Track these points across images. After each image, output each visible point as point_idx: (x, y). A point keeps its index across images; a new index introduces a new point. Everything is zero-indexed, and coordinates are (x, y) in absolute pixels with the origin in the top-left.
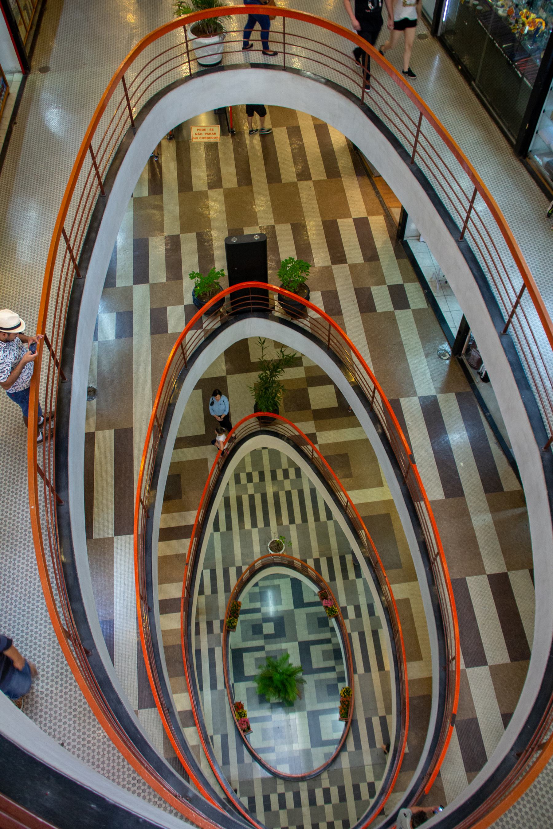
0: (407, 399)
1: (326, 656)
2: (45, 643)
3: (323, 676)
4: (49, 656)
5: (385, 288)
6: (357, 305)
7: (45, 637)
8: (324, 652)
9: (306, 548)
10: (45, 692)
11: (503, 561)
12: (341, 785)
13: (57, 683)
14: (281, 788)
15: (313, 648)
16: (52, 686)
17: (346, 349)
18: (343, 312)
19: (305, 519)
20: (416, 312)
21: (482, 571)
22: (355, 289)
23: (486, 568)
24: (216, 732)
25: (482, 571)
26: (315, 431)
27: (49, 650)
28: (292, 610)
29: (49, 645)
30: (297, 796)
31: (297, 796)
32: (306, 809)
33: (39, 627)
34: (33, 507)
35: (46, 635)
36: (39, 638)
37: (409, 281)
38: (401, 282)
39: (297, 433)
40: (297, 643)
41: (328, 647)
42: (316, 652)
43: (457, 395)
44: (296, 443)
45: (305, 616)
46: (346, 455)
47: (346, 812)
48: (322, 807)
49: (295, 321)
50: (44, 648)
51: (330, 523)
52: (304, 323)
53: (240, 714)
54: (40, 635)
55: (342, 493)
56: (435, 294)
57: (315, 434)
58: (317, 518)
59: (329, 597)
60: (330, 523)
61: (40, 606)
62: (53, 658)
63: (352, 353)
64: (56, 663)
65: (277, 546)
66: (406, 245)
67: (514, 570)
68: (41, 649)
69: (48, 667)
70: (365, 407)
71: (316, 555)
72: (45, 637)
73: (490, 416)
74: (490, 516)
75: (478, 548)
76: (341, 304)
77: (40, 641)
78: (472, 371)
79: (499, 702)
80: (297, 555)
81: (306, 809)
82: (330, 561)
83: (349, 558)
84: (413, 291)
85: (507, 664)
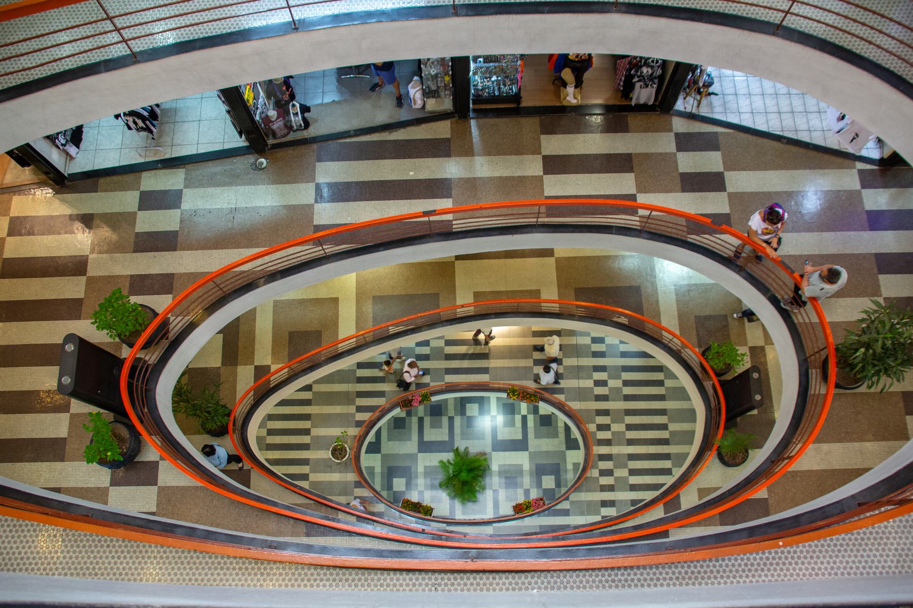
0: (315, 217)
1: (436, 425)
2: (841, 562)
3: (457, 430)
4: (856, 556)
5: (141, 214)
6: (162, 253)
7: (835, 563)
8: (433, 426)
9: (343, 420)
10: (898, 557)
11: (530, 157)
12: (594, 413)
13: (886, 544)
14: (595, 473)
15: (427, 438)
16: (890, 550)
17: (229, 275)
18: (169, 272)
19: (306, 417)
20: (188, 184)
21: (540, 179)
22: (135, 251)
23: (536, 174)
24: (598, 513)
25: (540, 179)
26: (253, 367)
27: (850, 556)
28: (382, 456)
29: (843, 557)
30: (603, 457)
31: (603, 457)
32: (614, 450)
33: (823, 571)
34: (781, 543)
35: (831, 561)
36: (836, 570)
37: (139, 184)
38: (137, 194)
39: (252, 393)
40: (420, 455)
41: (427, 421)
42: (431, 435)
43: (319, 160)
44: (262, 394)
45: (390, 443)
46: (290, 333)
47: (618, 411)
48: (613, 433)
49: (172, 335)
50: (847, 562)
51: (316, 388)
52: (177, 324)
53: (527, 507)
54: (832, 568)
55: (340, 345)
56: (168, 156)
57: (256, 367)
58: (307, 402)
59: (410, 398)
60: (316, 388)
61: (798, 571)
62: (858, 551)
63: (236, 269)
64: (864, 547)
65: (338, 452)
66: (75, 177)
67: (540, 148)
68: (848, 566)
69: (869, 556)
70: (321, 265)
71: (352, 409)
72: (835, 563)
73: (355, 131)
74: (477, 158)
75: (513, 177)
76: (155, 272)
77: (839, 568)
78: (292, 137)
79: (671, 192)
80: (353, 431)
81: (614, 450)
82: (361, 394)
83: (361, 373)
84: (152, 182)
85: (636, 177)
